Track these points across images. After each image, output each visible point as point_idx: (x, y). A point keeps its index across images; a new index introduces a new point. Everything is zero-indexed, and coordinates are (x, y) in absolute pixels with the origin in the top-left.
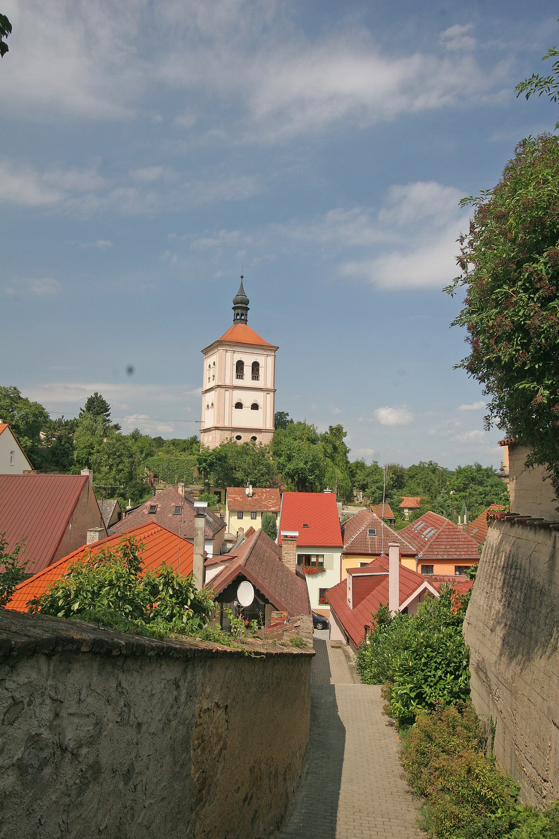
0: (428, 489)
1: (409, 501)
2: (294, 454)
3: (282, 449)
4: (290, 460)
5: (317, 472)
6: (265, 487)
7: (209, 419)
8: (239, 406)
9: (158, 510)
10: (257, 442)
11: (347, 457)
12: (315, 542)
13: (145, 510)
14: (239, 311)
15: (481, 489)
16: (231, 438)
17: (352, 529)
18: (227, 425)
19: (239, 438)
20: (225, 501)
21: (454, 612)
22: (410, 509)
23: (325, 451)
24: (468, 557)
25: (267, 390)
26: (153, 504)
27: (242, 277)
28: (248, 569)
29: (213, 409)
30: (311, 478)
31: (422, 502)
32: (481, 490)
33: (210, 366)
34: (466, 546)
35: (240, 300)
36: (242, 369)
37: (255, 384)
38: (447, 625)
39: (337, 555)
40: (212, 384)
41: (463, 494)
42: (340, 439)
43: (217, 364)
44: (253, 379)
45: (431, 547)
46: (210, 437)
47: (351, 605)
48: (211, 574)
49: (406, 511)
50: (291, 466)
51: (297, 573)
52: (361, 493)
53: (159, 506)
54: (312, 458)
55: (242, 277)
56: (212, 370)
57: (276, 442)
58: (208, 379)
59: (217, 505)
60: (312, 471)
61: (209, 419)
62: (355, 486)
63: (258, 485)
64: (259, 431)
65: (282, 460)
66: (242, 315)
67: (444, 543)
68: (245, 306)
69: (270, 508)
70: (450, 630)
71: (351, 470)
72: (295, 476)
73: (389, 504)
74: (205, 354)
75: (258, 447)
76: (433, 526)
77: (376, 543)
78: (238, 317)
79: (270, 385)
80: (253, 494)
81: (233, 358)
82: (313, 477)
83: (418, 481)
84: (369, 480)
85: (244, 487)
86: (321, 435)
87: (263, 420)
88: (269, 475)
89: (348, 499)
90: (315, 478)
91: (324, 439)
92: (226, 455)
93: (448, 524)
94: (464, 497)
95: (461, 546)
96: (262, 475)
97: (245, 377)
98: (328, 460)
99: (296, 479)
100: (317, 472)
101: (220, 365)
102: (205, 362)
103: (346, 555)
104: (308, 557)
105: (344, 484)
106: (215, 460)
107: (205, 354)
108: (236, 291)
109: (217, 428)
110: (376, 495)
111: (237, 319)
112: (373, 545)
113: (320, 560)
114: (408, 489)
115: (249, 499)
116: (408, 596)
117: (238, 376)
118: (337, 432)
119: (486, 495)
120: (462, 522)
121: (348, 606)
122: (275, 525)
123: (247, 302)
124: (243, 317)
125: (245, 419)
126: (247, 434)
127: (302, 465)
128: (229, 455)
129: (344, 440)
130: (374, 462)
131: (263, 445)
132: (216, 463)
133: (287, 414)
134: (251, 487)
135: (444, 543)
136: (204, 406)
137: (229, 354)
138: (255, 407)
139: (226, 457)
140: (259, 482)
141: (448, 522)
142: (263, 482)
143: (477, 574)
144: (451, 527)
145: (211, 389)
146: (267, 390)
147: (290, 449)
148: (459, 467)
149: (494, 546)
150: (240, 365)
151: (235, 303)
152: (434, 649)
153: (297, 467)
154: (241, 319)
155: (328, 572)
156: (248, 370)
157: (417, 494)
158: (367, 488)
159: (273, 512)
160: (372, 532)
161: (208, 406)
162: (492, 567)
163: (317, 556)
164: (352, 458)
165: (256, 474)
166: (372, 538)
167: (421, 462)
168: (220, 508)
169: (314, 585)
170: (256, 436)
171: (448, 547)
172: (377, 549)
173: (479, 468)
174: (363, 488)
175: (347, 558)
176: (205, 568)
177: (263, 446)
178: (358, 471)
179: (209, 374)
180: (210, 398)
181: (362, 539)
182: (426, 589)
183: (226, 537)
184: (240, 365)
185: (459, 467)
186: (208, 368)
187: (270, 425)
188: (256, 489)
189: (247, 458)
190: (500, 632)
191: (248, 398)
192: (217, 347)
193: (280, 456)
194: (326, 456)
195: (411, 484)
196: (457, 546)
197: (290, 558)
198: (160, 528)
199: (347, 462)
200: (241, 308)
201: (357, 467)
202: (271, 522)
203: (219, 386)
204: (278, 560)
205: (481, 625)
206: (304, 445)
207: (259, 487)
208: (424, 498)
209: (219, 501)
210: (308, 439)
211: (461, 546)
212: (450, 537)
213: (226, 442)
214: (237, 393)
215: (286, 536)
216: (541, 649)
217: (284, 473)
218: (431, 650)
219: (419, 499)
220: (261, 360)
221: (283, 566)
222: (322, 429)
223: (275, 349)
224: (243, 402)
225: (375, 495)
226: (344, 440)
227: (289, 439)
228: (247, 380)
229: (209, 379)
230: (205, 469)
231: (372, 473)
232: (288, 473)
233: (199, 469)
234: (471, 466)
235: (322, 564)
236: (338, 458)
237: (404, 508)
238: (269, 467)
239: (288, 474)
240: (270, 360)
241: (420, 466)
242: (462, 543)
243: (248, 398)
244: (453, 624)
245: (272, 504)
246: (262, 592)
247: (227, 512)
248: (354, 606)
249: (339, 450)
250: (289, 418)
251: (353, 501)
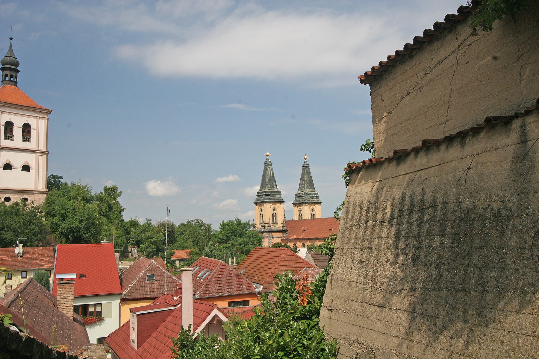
0: (196, 243)
1: (180, 254)
2: (68, 214)
4: (64, 220)
5: (92, 230)
6: (37, 246)
8: (8, 167)
10: (29, 202)
11: (121, 216)
12: (92, 291)
14: (8, 72)
15: (241, 240)
17: (131, 276)
19: (8, 199)
21: (302, 303)
23: (101, 210)
24: (239, 293)
25: (40, 153)
27: (11, 39)
30: (86, 236)
31: (191, 253)
32: (241, 241)
34: (238, 283)
38: (297, 320)
39: (116, 303)
41: (226, 245)
42: (115, 198)
45: (207, 286)
47: (135, 346)
49: (177, 262)
50: (65, 225)
51: (75, 320)
52: (136, 249)
54: (87, 217)
55: (11, 39)
57: (49, 203)
60: (87, 229)
62: (129, 243)
63: (29, 244)
64: (31, 192)
65: (55, 220)
66: (11, 76)
67: (218, 282)
68: (14, 67)
69: (43, 266)
70: (303, 325)
72: (69, 235)
73: (162, 257)
75: (30, 207)
77: (155, 287)
78: (7, 79)
80: (24, 253)
82: (88, 235)
83: (187, 237)
84: (143, 236)
85: (13, 247)
86: (95, 195)
87: (36, 181)
88: (41, 234)
89: (124, 255)
90: (90, 236)
91: (99, 198)
94: (227, 248)
95: (233, 284)
97: (15, 138)
98: (104, 219)
100: (92, 230)
103: (125, 301)
104: (85, 307)
105: (119, 241)
108: (5, 52)
110: (150, 250)
111: (5, 80)
113: (98, 309)
114: (178, 243)
115: (19, 258)
116: (204, 320)
117: (6, 136)
118: (112, 192)
120: (232, 263)
121: (131, 348)
123: (17, 64)
124: (12, 79)
127: (77, 224)
129: (119, 199)
130: (147, 220)
131: (35, 204)
133: (61, 177)
134: (21, 246)
135: (218, 282)
138: (26, 168)
140: (31, 242)
143: (336, 245)
144: (224, 267)
146: (40, 153)
147: (64, 209)
148: (223, 222)
149: (365, 201)
150: (9, 126)
151: (4, 63)
152: (287, 351)
153: (72, 226)
155: (107, 320)
156: (18, 132)
157: (187, 248)
159: (46, 270)
160: (150, 277)
163: (95, 305)
164: (127, 217)
165: (27, 234)
166: (151, 283)
169: (95, 333)
170: (28, 197)
171: (222, 285)
173: (239, 223)
174: (137, 244)
175: (126, 304)
177: (35, 206)
178: (132, 228)
185: (223, 222)
187: (42, 186)
188: (27, 249)
189: (18, 218)
193: (54, 216)
194: (101, 215)
196: (229, 284)
197: (67, 303)
201: (131, 225)
202: (44, 280)
204: (52, 306)
206: (79, 204)
207: (31, 246)
208: (193, 250)
210: (83, 199)
211: (233, 284)
212: (223, 276)
215: (62, 280)
216: (516, 301)
217: (57, 233)
218: (283, 353)
219: (188, 251)
220: (32, 122)
221: (58, 312)
222: (97, 190)
224: (12, 163)
225: (149, 250)
226: (119, 199)
227: (64, 200)
228: (17, 141)
232: (62, 232)
234: (233, 221)
235: (100, 313)
236: (113, 216)
237: (175, 260)
239: (62, 233)
245: (45, 262)
248: (139, 346)
249: (114, 209)
250: (62, 181)
251: (128, 257)
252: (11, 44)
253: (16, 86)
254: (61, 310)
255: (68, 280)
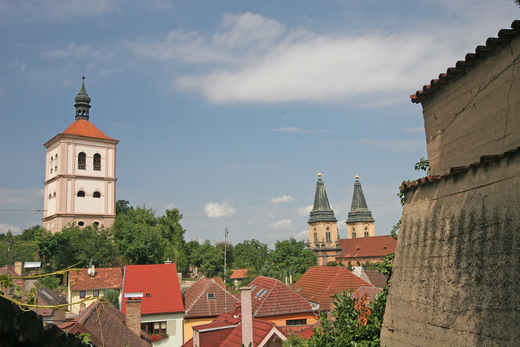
0: (253, 262)
2: (134, 236)
3: (123, 232)
4: (131, 242)
5: (156, 251)
6: (107, 267)
7: (51, 208)
8: (81, 194)
10: (99, 226)
11: (183, 238)
14: (81, 108)
15: (296, 259)
16: (73, 224)
17: (192, 295)
18: (69, 212)
19: (81, 224)
20: (68, 283)
22: (239, 279)
24: (297, 311)
25: (109, 180)
27: (84, 78)
29: (55, 198)
30: (151, 257)
31: (249, 272)
32: (296, 260)
33: (52, 158)
34: (294, 302)
35: (81, 98)
36: (84, 160)
37: (97, 174)
39: (179, 321)
40: (55, 174)
43: (59, 156)
46: (53, 225)
49: (236, 281)
50: (131, 247)
51: (142, 337)
52: (196, 269)
55: (84, 78)
56: (54, 161)
57: (117, 226)
58: (50, 171)
59: (59, 287)
60: (151, 251)
61: (51, 208)
62: (190, 263)
63: (100, 265)
64: (101, 217)
65: (123, 242)
66: (84, 112)
69: (112, 285)
71: (187, 249)
73: (221, 276)
74: (47, 147)
75: (101, 230)
76: (265, 287)
77: (216, 306)
78: (80, 114)
79: (111, 175)
80: (96, 274)
81: (75, 151)
82: (153, 256)
83: (244, 256)
84: (203, 256)
85: (86, 268)
87: (105, 206)
88: (111, 256)
89: (186, 275)
90: (155, 257)
91: (162, 221)
92: (68, 238)
93: (279, 284)
96: (105, 256)
97: (87, 167)
98: (166, 240)
99: (137, 258)
101: (62, 157)
102: (48, 155)
103: (188, 319)
104: (151, 325)
105: (181, 262)
106: (56, 243)
107: (47, 147)
108: (79, 90)
109: (59, 215)
110: (210, 269)
111: (79, 116)
112: (212, 308)
113: (163, 327)
114: (236, 263)
115: (92, 278)
116: (263, 338)
117: (80, 166)
118: (174, 215)
119: (301, 264)
120: (289, 282)
122: (117, 301)
123: (89, 101)
124: (85, 114)
125: (87, 206)
127: (142, 245)
128: (71, 238)
129: (180, 222)
130: (206, 241)
131: (105, 227)
132: (58, 246)
134: (93, 267)
136: (47, 196)
137: (71, 147)
138: (97, 195)
139: (68, 240)
140: (102, 263)
141: (278, 282)
142: (106, 262)
144: (280, 286)
146: (109, 180)
147: (130, 232)
149: (423, 220)
150: (82, 157)
151: (77, 100)
153: (138, 247)
155: (171, 338)
156: (89, 162)
157: (244, 267)
158: (202, 263)
159: (115, 289)
161: (50, 195)
162: (425, 246)
163: (160, 323)
164: (188, 238)
166: (212, 302)
167: (245, 241)
168: (62, 290)
171: (279, 304)
172: (216, 311)
173: (294, 242)
174: (198, 264)
175: (189, 322)
177: (105, 229)
179: (52, 165)
180: (52, 187)
181: (202, 303)
182: (274, 334)
184: (82, 157)
185: (278, 242)
186: (50, 160)
187: (111, 211)
189: (90, 241)
190: (466, 324)
191: (90, 187)
192: (59, 139)
193: (122, 238)
194: (164, 237)
195: (238, 259)
196: (287, 303)
199: (184, 242)
200: (83, 105)
201: (192, 246)
202: (114, 298)
203: (61, 176)
204: (122, 324)
205: (419, 326)
206: (144, 227)
207: (102, 267)
208: (250, 269)
209: (61, 283)
210: (148, 222)
212: (280, 294)
213: (68, 227)
215: (130, 298)
217: (125, 254)
219: (246, 270)
220: (102, 152)
221: (127, 329)
222: (160, 213)
223: (116, 142)
225: (208, 269)
226: (180, 222)
227: (130, 223)
228: (89, 170)
229: (52, 170)
230: (46, 253)
231: (205, 251)
232: (129, 254)
233: (40, 253)
234: (288, 241)
235: (165, 330)
236: (175, 237)
238: (111, 248)
239: (129, 255)
240: (111, 152)
241: (245, 244)
242: (291, 299)
244: (365, 338)
245: (115, 282)
247: (69, 292)
249: (176, 231)
250: (129, 206)
251: (189, 276)
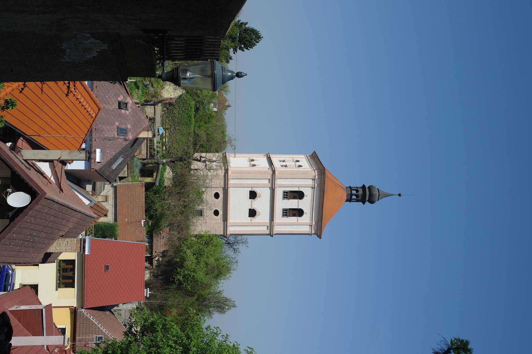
8: (253, 195)
9: (123, 111)
13: (122, 97)
14: (361, 192)
18: (231, 182)
26: (129, 105)
28: (43, 201)
36: (294, 198)
37: (278, 212)
44: (284, 210)
48: (45, 167)
53: (127, 112)
55: (399, 195)
56: (293, 163)
58: (283, 159)
64: (225, 218)
66: (357, 196)
68: (367, 198)
79: (277, 229)
97: (286, 201)
101: (296, 171)
102: (303, 156)
103: (74, 312)
108: (384, 189)
117: (287, 193)
121: (13, 306)
123: (372, 202)
124: (354, 197)
125: (239, 202)
126: (221, 205)
137: (310, 182)
138: (252, 213)
145: (271, 163)
150: (300, 195)
154: (352, 195)
156: (293, 204)
161: (253, 160)
170: (219, 216)
175: (71, 313)
176: (51, 161)
179: (289, 161)
180: (262, 162)
183: (98, 184)
184: (300, 195)
191: (262, 205)
198: (94, 115)
200: (364, 195)
203: (274, 172)
204: (61, 234)
214: (268, 191)
215: (84, 242)
220: (306, 219)
223: (319, 233)
224: (257, 199)
228: (282, 204)
229: (284, 161)
240: (306, 229)
243: (262, 205)
246: (21, 215)
252: (394, 195)
253: (347, 201)
254: (56, 241)
255: (84, 247)
